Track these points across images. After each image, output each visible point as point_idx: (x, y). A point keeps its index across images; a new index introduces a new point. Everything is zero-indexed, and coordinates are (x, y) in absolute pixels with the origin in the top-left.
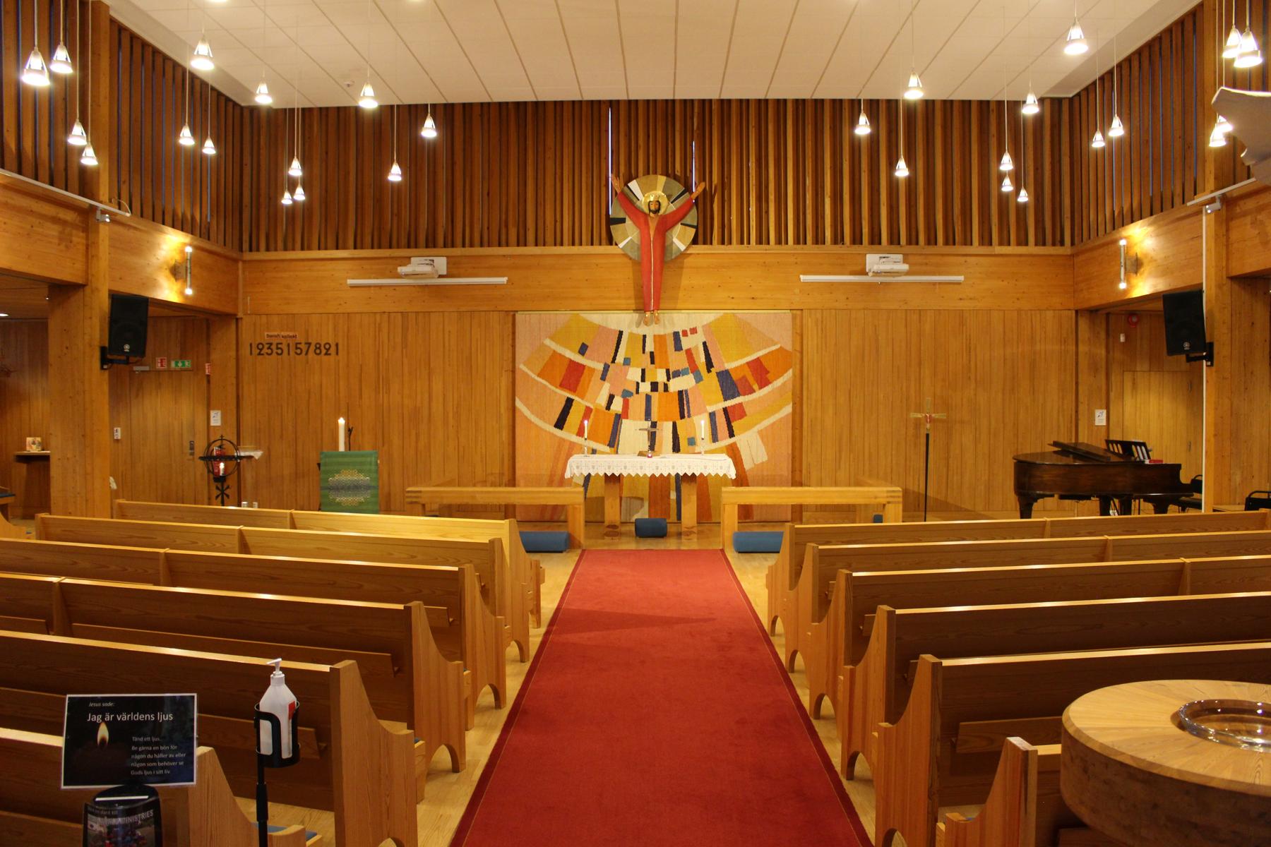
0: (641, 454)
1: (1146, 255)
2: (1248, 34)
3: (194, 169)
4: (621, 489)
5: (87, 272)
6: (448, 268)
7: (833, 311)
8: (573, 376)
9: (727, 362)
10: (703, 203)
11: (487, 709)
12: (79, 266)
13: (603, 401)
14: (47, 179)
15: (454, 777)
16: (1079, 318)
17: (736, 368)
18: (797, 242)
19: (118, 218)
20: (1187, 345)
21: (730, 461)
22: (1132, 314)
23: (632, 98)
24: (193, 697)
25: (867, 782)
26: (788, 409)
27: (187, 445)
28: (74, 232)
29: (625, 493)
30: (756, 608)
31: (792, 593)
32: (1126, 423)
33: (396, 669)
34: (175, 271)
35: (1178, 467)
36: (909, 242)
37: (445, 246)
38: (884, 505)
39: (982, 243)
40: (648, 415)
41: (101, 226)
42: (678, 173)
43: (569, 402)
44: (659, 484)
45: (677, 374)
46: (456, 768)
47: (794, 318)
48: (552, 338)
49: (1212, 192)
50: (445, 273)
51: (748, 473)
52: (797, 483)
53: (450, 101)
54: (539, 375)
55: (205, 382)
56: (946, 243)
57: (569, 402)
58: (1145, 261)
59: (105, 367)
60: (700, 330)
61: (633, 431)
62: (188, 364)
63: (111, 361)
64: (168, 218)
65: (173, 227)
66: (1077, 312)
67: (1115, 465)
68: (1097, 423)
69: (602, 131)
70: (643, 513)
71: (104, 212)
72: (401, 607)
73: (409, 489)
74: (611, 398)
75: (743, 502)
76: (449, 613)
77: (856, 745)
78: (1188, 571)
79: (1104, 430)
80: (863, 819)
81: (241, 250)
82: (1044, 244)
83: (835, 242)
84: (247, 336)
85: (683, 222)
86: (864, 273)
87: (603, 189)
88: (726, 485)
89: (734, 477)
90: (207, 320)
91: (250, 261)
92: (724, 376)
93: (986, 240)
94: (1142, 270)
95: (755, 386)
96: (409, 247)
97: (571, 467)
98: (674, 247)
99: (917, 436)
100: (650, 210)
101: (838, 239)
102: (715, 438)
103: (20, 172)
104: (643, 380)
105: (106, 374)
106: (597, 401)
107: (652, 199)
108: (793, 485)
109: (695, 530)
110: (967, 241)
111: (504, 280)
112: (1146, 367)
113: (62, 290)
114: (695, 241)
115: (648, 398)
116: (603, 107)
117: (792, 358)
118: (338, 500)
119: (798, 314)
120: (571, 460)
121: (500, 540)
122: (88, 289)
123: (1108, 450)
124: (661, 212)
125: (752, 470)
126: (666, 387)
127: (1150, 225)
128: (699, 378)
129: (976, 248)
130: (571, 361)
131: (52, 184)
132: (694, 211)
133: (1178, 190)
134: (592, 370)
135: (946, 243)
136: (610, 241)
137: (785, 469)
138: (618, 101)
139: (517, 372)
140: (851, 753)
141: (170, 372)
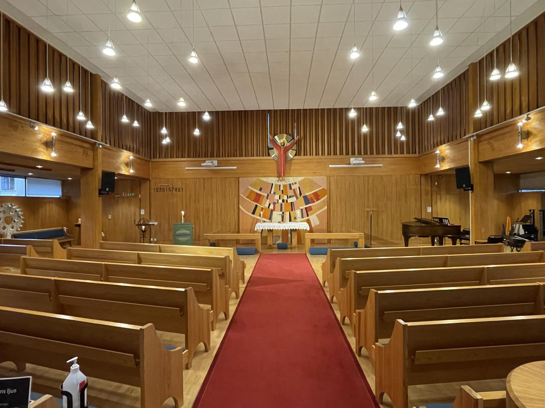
0: (279, 222)
1: (446, 156)
2: (512, 64)
3: (134, 132)
4: (273, 233)
5: (94, 164)
6: (218, 164)
7: (340, 177)
8: (258, 198)
9: (307, 193)
10: (298, 143)
11: (222, 320)
12: (91, 162)
13: (267, 205)
14: (79, 133)
15: (206, 354)
16: (422, 177)
17: (309, 195)
18: (328, 154)
19: (105, 146)
20: (464, 186)
21: (307, 224)
22: (439, 175)
23: (275, 109)
24: (29, 378)
25: (367, 357)
26: (326, 208)
27: (133, 220)
28: (89, 151)
29: (274, 235)
30: (318, 276)
31: (332, 274)
32: (438, 211)
33: (182, 314)
34: (127, 165)
35: (460, 226)
36: (364, 154)
37: (217, 157)
38: (358, 239)
39: (388, 154)
40: (281, 210)
41: (99, 149)
42: (290, 133)
43: (256, 206)
44: (285, 232)
45: (290, 197)
46: (206, 351)
47: (327, 179)
48: (251, 186)
49: (473, 133)
50: (217, 165)
51: (313, 229)
52: (329, 232)
53: (217, 110)
54: (247, 198)
55: (139, 200)
56: (377, 154)
57: (256, 206)
58: (446, 158)
59: (100, 196)
60: (297, 183)
61: (277, 215)
62: (133, 195)
63: (103, 194)
64: (124, 147)
65: (126, 150)
66: (420, 175)
67: (438, 226)
68: (428, 211)
69: (266, 120)
70: (280, 241)
71: (99, 144)
72: (183, 290)
73: (204, 235)
74: (270, 204)
75: (312, 238)
76: (207, 286)
77: (362, 343)
78: (486, 271)
79: (430, 214)
80: (368, 379)
81: (151, 158)
82: (409, 153)
83: (340, 154)
84: (153, 186)
85: (292, 149)
86: (350, 164)
87: (267, 139)
88: (306, 233)
89: (309, 230)
90: (140, 181)
91: (154, 162)
92: (305, 198)
93: (390, 152)
94: (445, 161)
95: (315, 201)
96: (205, 157)
97: (257, 227)
98: (289, 157)
99: (368, 216)
100: (281, 145)
101: (341, 153)
102: (303, 217)
103: (68, 130)
104: (280, 199)
105: (101, 198)
106: (265, 206)
107: (282, 141)
108: (328, 232)
109: (296, 247)
110: (383, 153)
111: (235, 167)
112: (445, 193)
113: (85, 170)
114: (296, 155)
115: (281, 205)
116: (267, 112)
117: (327, 192)
118: (179, 239)
119: (329, 178)
120: (257, 224)
121: (229, 256)
122: (94, 170)
123: (434, 220)
124: (285, 146)
125: (314, 227)
126: (287, 201)
127: (448, 145)
128: (297, 198)
129: (386, 155)
130: (257, 193)
131: (80, 135)
132: (295, 145)
133: (459, 133)
134: (264, 196)
135: (377, 154)
136: (269, 155)
137: (325, 227)
138: (271, 110)
139: (240, 197)
140: (360, 346)
141: (127, 197)
